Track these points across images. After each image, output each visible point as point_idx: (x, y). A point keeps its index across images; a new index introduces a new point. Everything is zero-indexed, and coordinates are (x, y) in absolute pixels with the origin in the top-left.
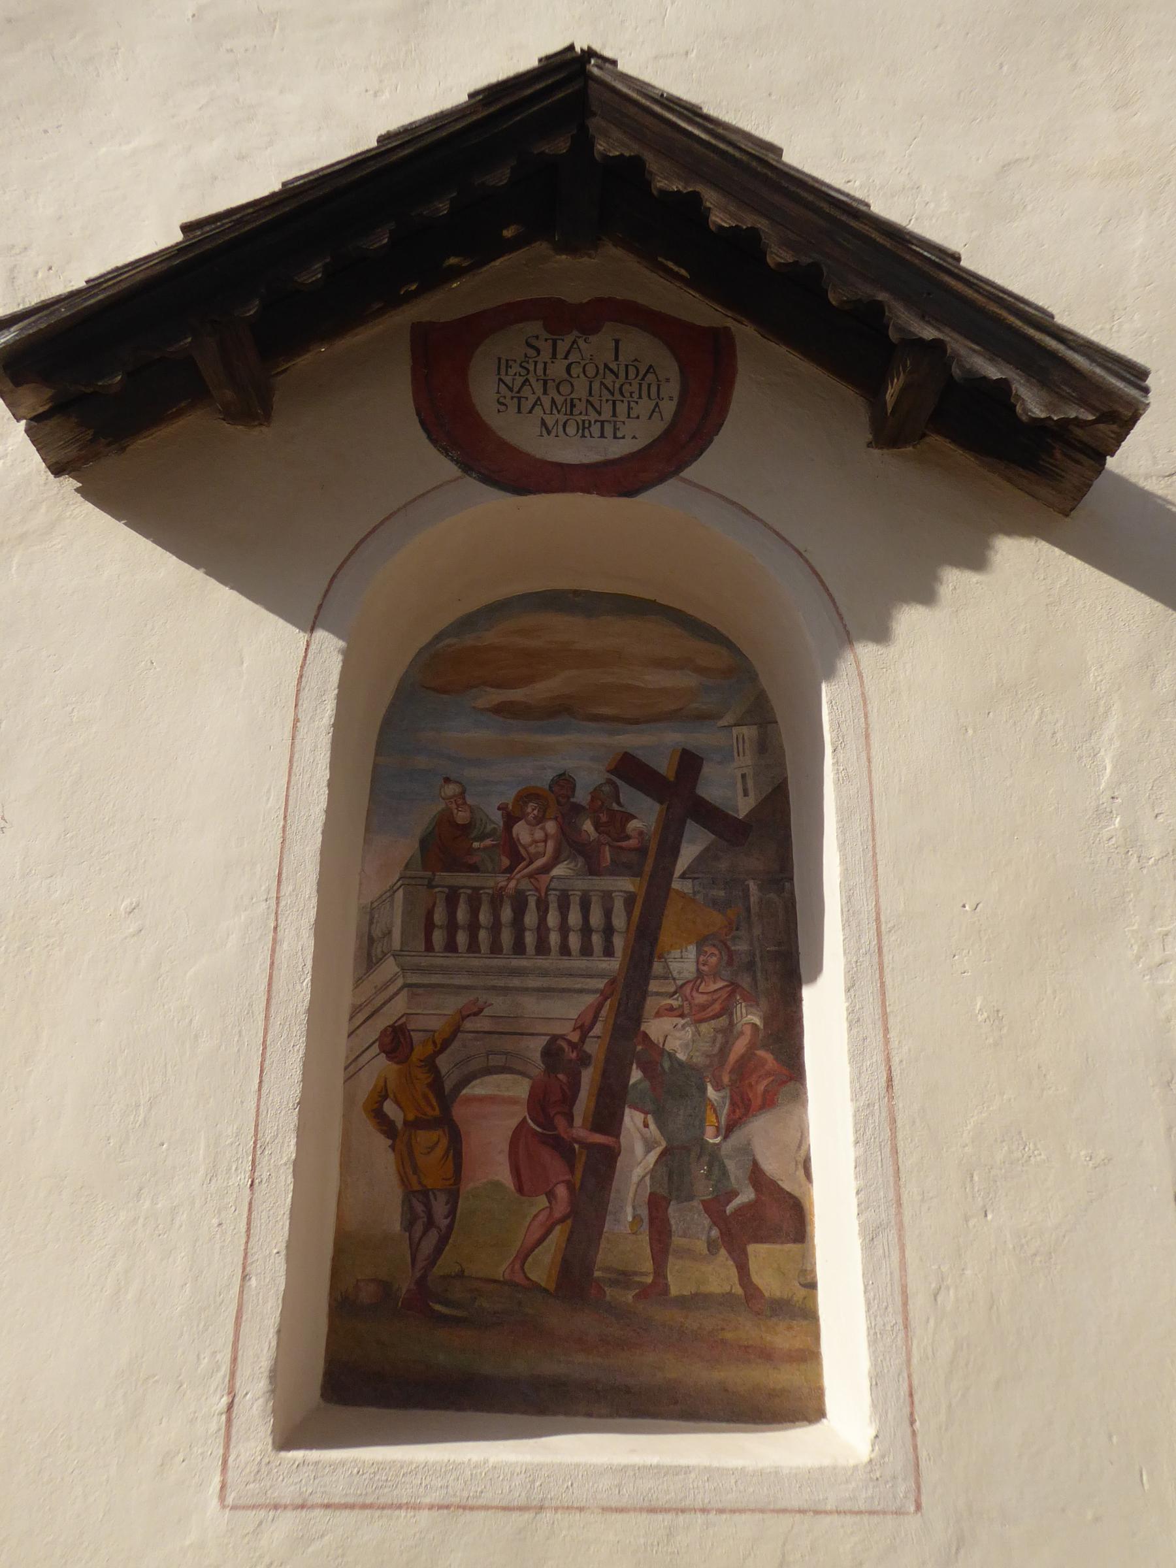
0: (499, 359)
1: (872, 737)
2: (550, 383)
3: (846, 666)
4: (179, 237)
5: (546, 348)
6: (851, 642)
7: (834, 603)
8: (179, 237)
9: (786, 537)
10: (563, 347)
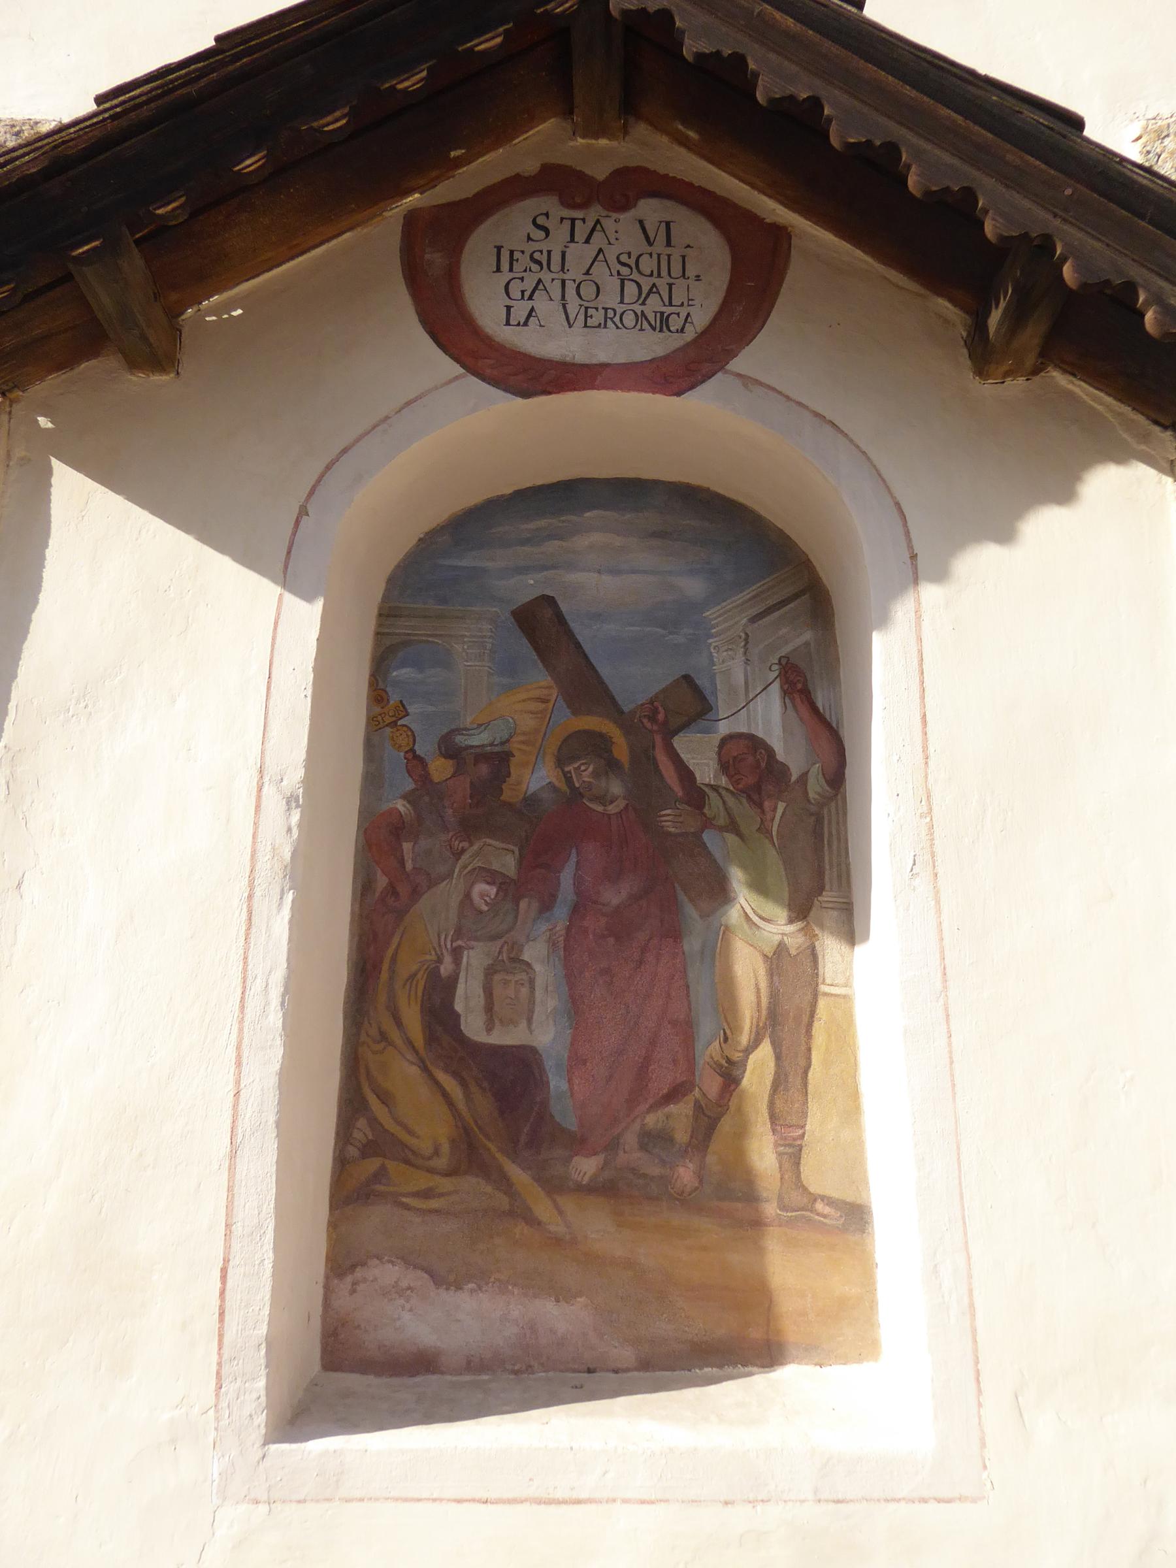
0: (499, 248)
1: (791, 395)
2: (569, 284)
3: (902, 611)
4: (92, 107)
5: (561, 234)
6: (916, 581)
7: (868, 459)
8: (92, 107)
9: (887, 480)
10: (581, 231)
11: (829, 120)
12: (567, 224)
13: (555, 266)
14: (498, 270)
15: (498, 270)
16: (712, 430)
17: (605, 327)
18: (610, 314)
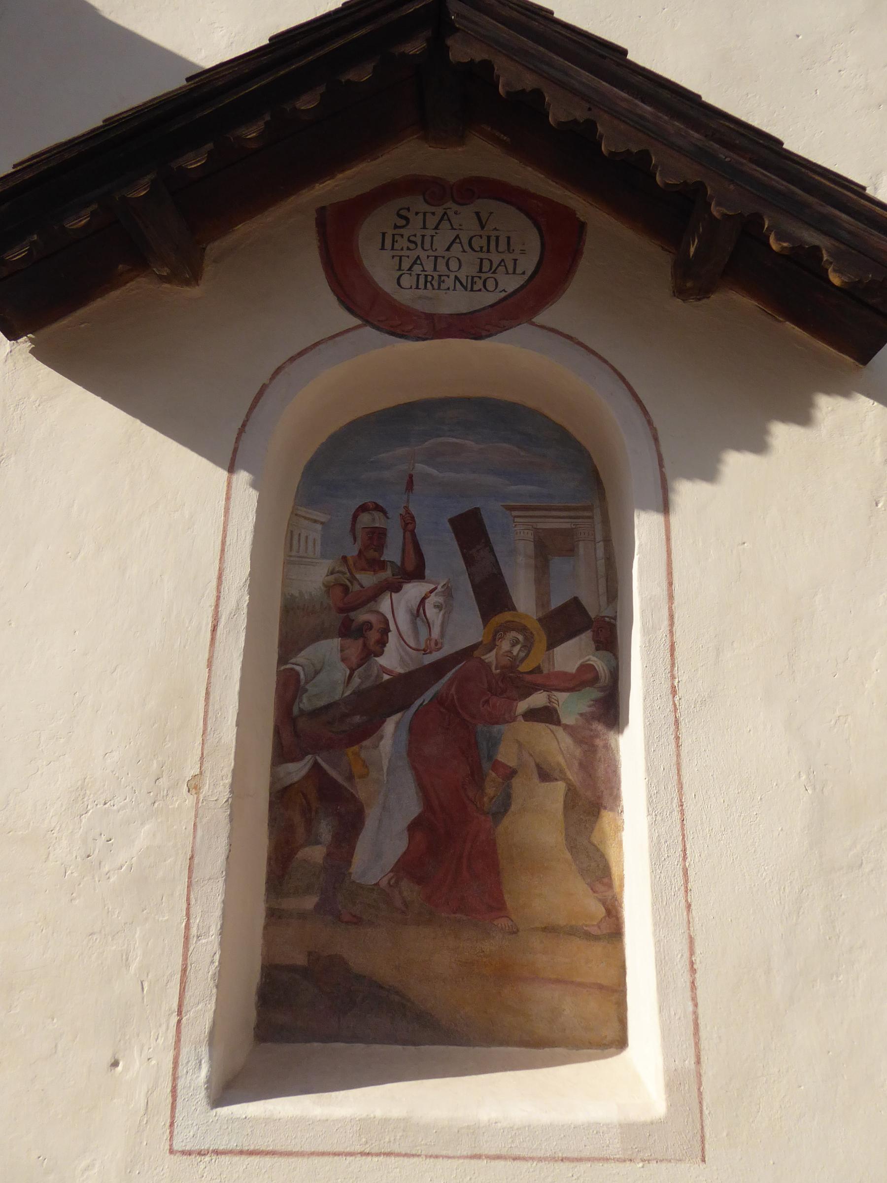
4: (101, 123)
11: (601, 136)
12: (421, 216)
13: (427, 245)
14: (383, 248)
15: (383, 248)
16: (517, 361)
17: (454, 289)
18: (429, 278)
